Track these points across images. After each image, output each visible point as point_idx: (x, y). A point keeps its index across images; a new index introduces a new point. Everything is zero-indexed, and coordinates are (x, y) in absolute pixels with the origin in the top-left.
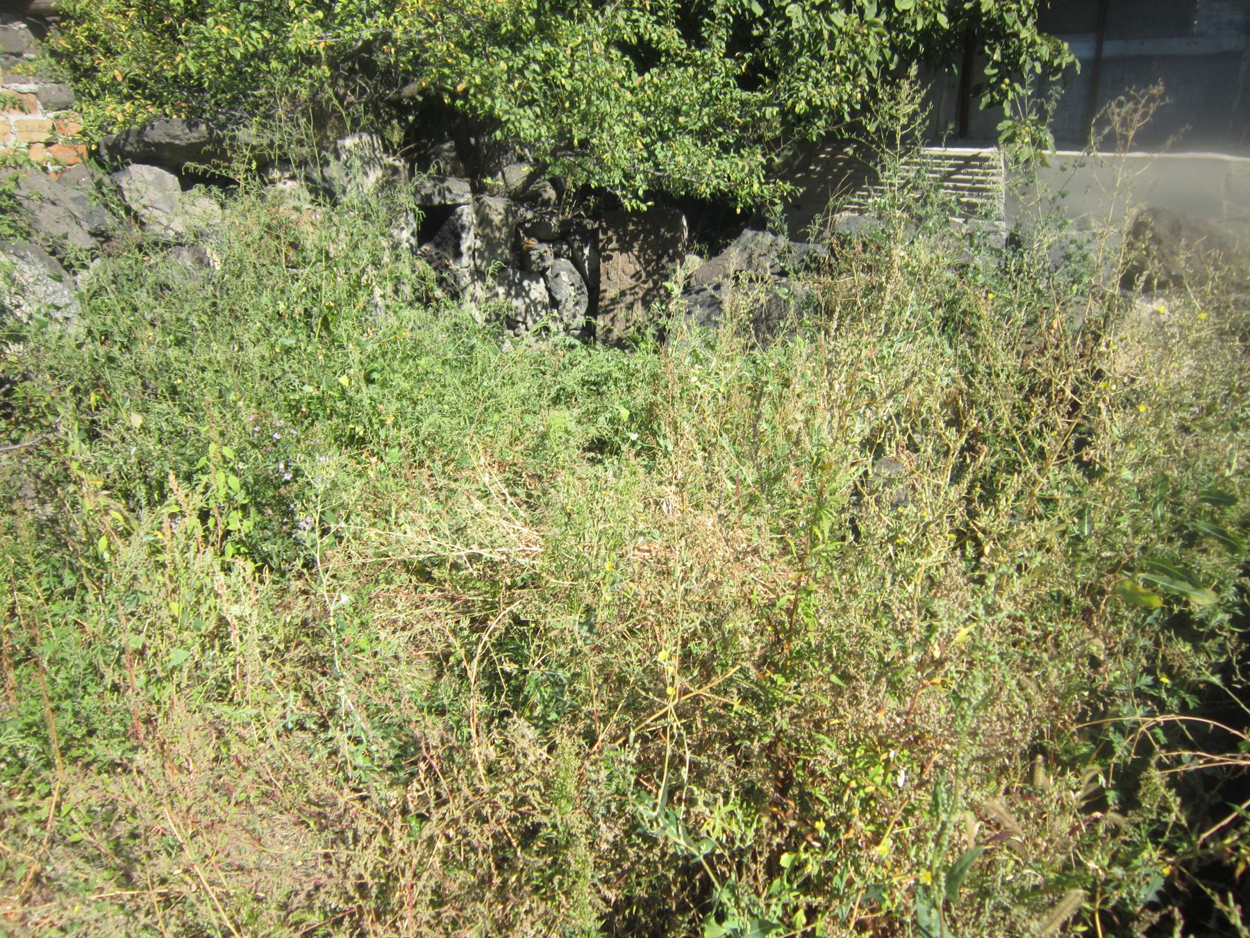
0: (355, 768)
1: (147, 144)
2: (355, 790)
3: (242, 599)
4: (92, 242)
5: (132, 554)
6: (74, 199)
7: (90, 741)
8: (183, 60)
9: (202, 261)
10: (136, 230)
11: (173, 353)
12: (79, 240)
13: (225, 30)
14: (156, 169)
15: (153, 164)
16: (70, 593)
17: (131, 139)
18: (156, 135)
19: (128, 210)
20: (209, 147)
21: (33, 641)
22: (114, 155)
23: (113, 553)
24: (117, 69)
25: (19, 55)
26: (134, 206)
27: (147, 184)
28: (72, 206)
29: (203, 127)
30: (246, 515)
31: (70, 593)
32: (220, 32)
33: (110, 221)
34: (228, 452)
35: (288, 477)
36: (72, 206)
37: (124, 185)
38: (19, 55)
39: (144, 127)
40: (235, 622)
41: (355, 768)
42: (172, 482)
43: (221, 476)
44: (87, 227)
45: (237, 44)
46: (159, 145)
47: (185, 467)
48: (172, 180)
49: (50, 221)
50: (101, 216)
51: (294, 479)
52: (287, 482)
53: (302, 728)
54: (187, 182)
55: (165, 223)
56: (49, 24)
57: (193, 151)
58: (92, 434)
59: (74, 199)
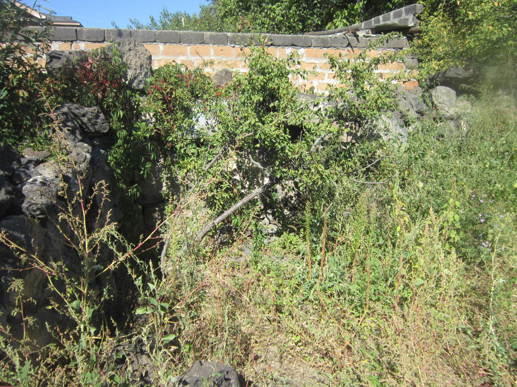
0: (489, 360)
1: (447, 78)
2: (486, 370)
3: (451, 269)
4: (417, 115)
5: (409, 236)
6: (413, 99)
7: (377, 303)
8: (469, 42)
9: (458, 127)
10: (434, 112)
11: (440, 161)
12: (412, 115)
13: (491, 28)
14: (448, 88)
15: (447, 86)
16: (380, 246)
17: (440, 76)
18: (451, 74)
19: (433, 103)
20: (472, 79)
21: (365, 259)
22: (432, 83)
23: (401, 234)
24: (440, 50)
25: (401, 49)
26: (435, 103)
27: (442, 94)
28: (412, 101)
29: (471, 71)
30: (458, 232)
31: (380, 246)
32: (489, 29)
33: (425, 107)
34: (458, 204)
35: (482, 221)
36: (412, 101)
37: (433, 94)
38: (401, 49)
39: (446, 71)
40: (445, 276)
41: (489, 360)
42: (431, 211)
43: (452, 213)
44: (415, 109)
45: (495, 34)
46: (451, 78)
47: (436, 208)
48: (453, 92)
49: (403, 106)
50: (422, 106)
51: (485, 222)
52: (481, 223)
53: (465, 332)
54: (459, 93)
55: (447, 110)
56: (414, 37)
57: (465, 80)
58: (402, 186)
59: (413, 99)
